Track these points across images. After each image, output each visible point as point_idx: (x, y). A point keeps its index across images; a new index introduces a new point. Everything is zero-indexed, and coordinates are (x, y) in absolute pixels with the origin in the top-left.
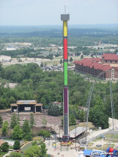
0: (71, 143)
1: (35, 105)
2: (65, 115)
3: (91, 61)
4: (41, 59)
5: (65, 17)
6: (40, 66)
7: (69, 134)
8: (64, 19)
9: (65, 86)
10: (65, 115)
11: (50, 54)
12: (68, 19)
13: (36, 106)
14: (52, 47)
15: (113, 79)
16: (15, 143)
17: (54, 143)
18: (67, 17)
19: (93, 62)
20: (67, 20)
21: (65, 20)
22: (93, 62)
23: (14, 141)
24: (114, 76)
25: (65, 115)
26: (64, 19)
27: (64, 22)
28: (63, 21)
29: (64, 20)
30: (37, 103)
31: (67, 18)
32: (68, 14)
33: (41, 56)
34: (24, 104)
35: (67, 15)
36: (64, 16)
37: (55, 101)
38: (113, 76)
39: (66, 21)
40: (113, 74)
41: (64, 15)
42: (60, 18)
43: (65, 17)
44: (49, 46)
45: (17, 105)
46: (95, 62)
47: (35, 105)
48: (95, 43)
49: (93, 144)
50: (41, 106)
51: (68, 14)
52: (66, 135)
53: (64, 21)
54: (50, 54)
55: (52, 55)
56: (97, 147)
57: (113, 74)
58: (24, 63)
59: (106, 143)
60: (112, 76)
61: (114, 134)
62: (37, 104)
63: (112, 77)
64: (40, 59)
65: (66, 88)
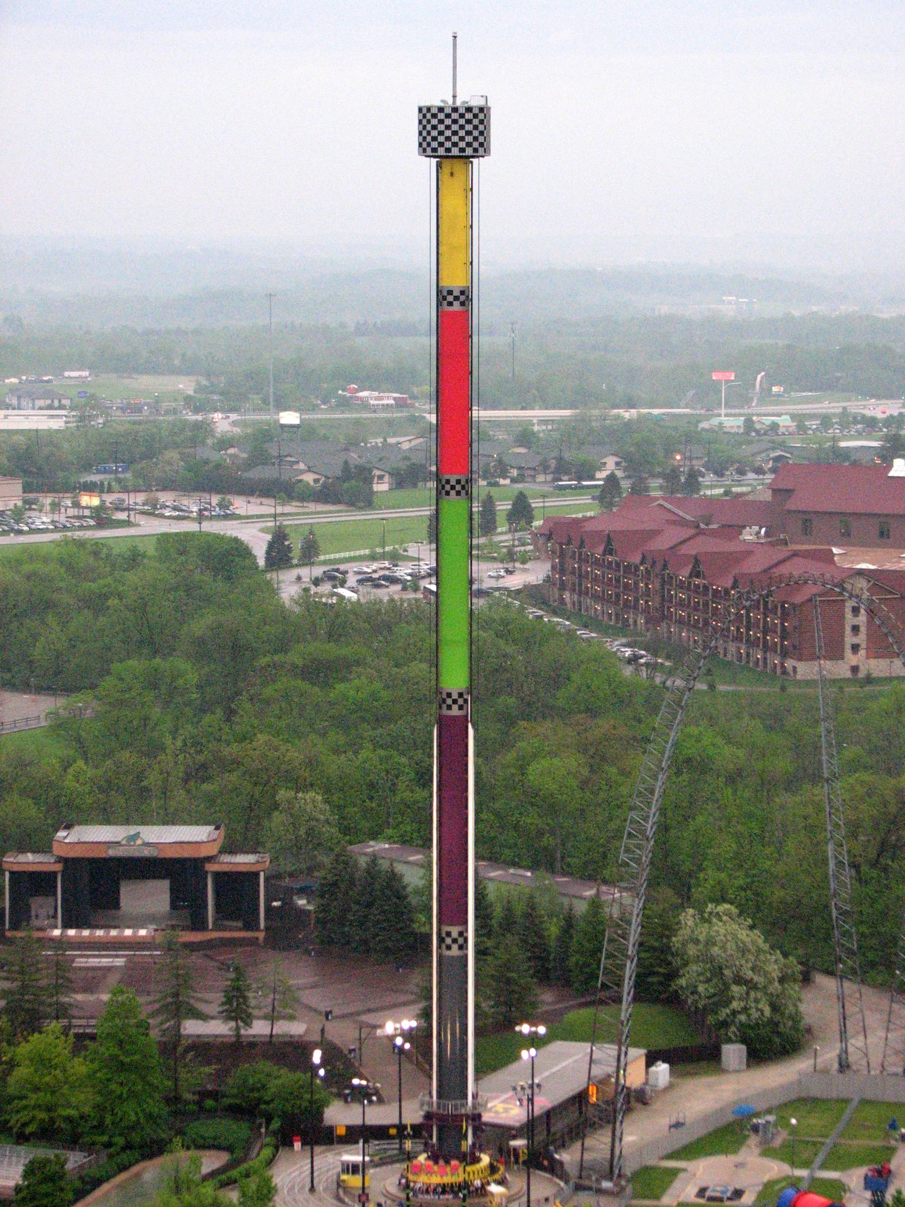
0: (493, 1169)
1: (211, 867)
2: (448, 941)
3: (683, 523)
4: (271, 501)
5: (455, 127)
6: (261, 562)
7: (475, 1097)
8: (448, 145)
9: (442, 698)
10: (441, 940)
11: (346, 462)
12: (481, 147)
13: (217, 875)
14: (365, 406)
15: (855, 669)
16: (29, 1172)
17: (354, 1169)
18: (469, 127)
19: (697, 531)
20: (469, 151)
21: (455, 151)
22: (697, 531)
23: (22, 1149)
24: (861, 639)
25: (449, 934)
26: (448, 145)
27: (446, 170)
28: (439, 166)
29: (441, 151)
30: (224, 850)
31: (469, 139)
32: (476, 103)
33: (276, 482)
34: (112, 853)
35: (469, 109)
36: (441, 127)
37: (374, 835)
38: (856, 640)
39: (458, 166)
40: (855, 629)
41: (441, 110)
42: (415, 139)
43: (455, 127)
44: (345, 404)
45: (58, 867)
46: (783, 585)
47: (211, 867)
48: (719, 382)
49: (424, 786)
50: (257, 874)
51: (481, 103)
52: (450, 1106)
53: (446, 164)
54: (346, 462)
55: (364, 475)
56: (702, 1201)
57: (855, 629)
58: (132, 531)
59: (776, 1169)
60: (849, 639)
61: (846, 1101)
62: (226, 858)
63: (848, 647)
64: (265, 501)
65: (455, 711)
